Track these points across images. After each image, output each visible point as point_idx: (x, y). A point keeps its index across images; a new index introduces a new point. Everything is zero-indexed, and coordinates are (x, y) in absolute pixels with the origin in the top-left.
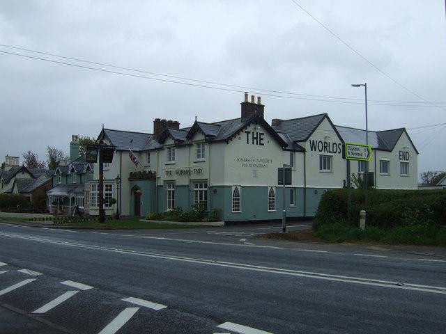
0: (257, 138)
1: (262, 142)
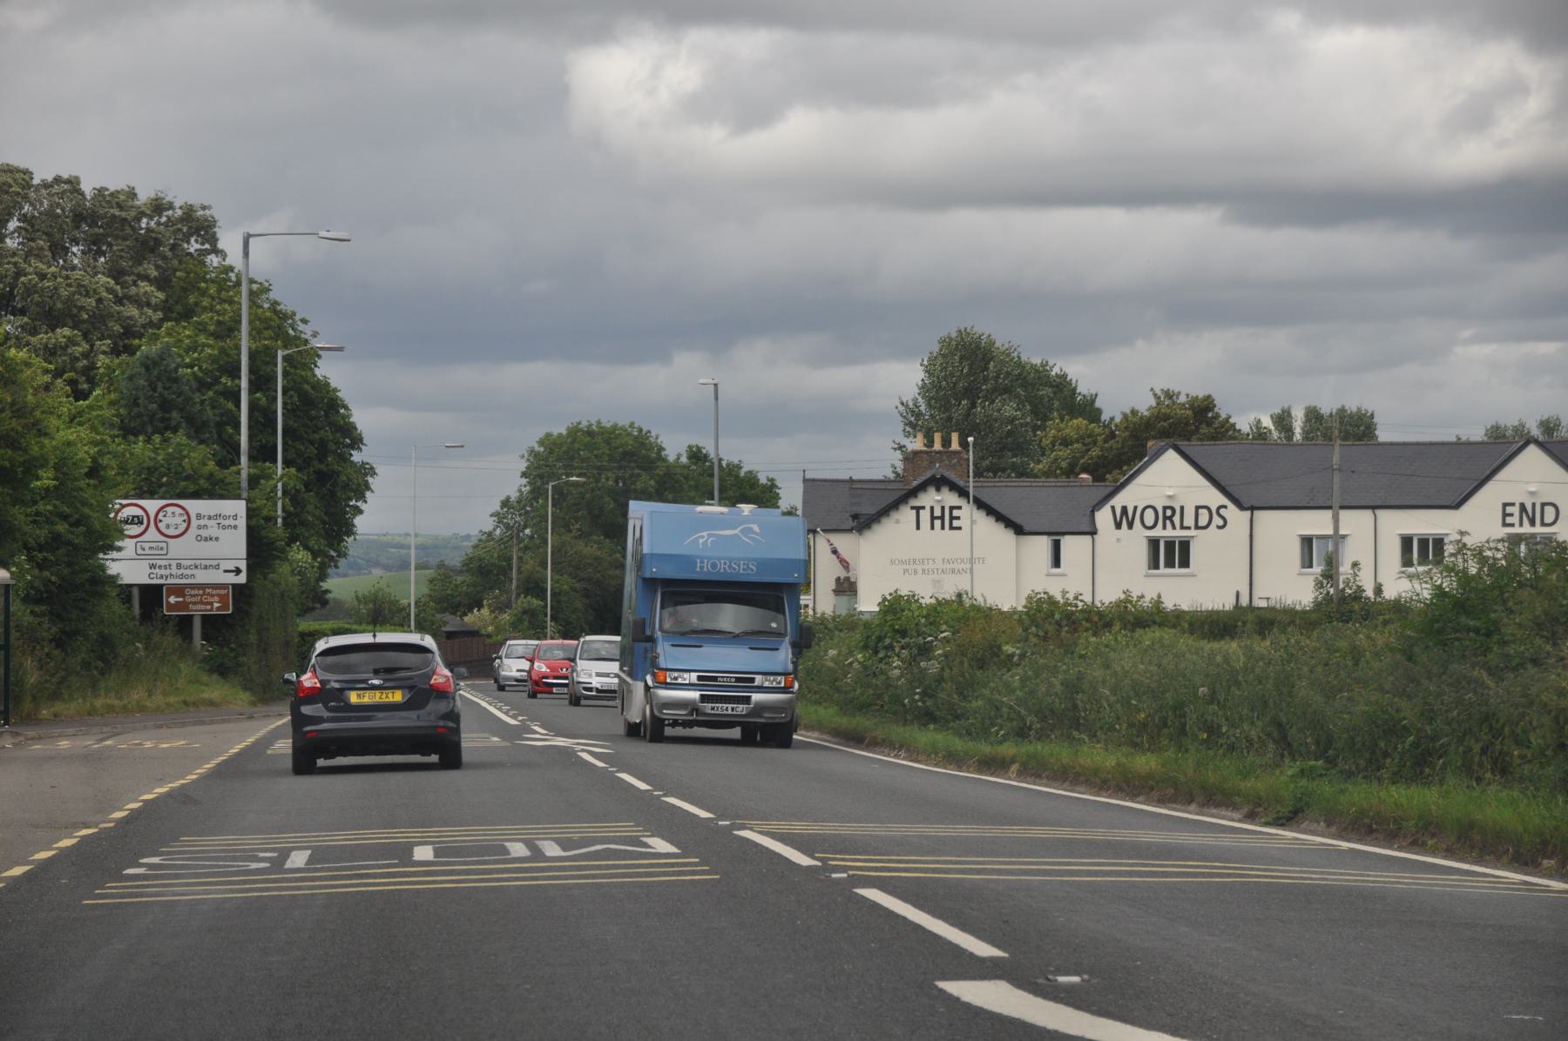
0: (942, 518)
1: (956, 523)
